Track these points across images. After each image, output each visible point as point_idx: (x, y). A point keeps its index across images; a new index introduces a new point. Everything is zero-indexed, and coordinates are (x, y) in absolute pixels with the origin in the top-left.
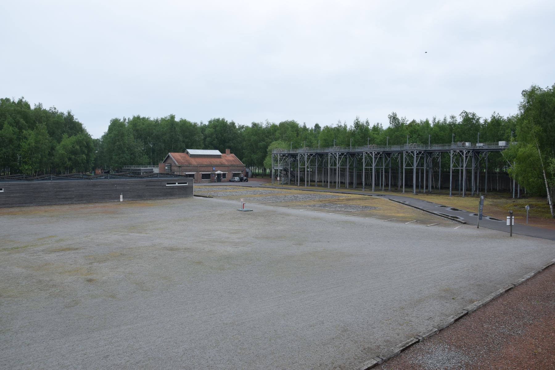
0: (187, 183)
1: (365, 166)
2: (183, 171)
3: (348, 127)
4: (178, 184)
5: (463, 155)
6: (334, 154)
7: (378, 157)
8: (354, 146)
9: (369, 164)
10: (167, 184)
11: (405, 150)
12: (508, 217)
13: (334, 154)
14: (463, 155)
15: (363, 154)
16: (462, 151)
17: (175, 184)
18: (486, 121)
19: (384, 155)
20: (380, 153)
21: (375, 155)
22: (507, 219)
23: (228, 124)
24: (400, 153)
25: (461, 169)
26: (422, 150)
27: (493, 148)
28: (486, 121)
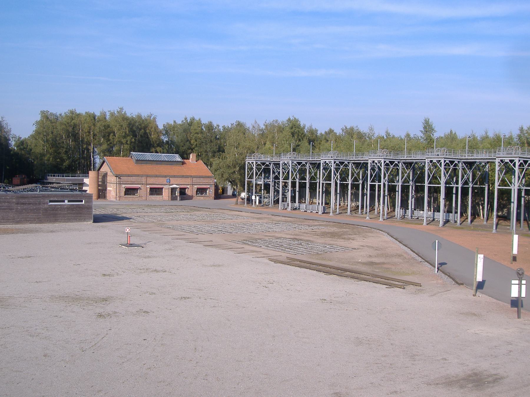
0: (84, 201)
1: (430, 183)
2: (121, 183)
3: (319, 132)
4: (69, 201)
5: (441, 166)
6: (251, 163)
7: (450, 168)
8: (409, 151)
9: (435, 179)
10: (51, 201)
11: (247, 161)
12: (514, 282)
13: (251, 163)
14: (515, 168)
15: (425, 163)
16: (513, 160)
17: (64, 201)
18: (321, 134)
19: (460, 165)
20: (454, 161)
21: (445, 165)
22: (522, 285)
23: (13, 143)
24: (488, 162)
25: (64, 176)
26: (455, 159)
27: (305, 160)
28: (321, 134)
